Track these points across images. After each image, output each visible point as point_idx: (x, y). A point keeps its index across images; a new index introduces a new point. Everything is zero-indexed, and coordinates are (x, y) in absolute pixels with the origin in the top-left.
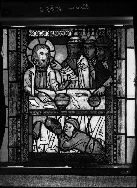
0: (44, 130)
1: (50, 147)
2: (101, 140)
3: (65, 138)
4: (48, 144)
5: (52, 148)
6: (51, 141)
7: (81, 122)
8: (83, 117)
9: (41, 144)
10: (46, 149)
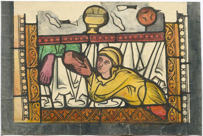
0: (62, 71)
3: (99, 81)
4: (70, 93)
5: (78, 99)
6: (75, 88)
8: (129, 44)
9: (59, 94)
10: (67, 101)
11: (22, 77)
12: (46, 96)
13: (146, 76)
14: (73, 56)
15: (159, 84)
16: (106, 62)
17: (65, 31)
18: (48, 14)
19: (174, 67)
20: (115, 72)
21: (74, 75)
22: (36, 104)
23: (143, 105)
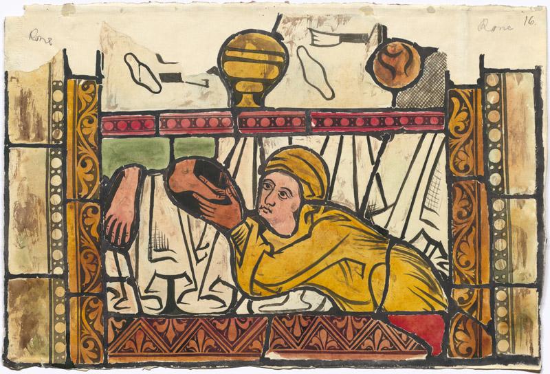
1: (195, 289)
2: (430, 241)
5: (206, 292)
7: (374, 29)
8: (348, 139)
9: (156, 275)
10: (176, 298)
11: (54, 103)
12: (121, 279)
13: (395, 230)
14: (197, 172)
15: (428, 254)
16: (284, 193)
17: (171, 98)
18: (131, 54)
19: (469, 123)
20: (309, 218)
21: (198, 225)
22: (91, 207)
23: (381, 313)
